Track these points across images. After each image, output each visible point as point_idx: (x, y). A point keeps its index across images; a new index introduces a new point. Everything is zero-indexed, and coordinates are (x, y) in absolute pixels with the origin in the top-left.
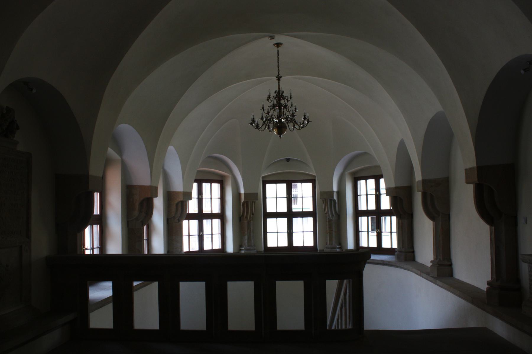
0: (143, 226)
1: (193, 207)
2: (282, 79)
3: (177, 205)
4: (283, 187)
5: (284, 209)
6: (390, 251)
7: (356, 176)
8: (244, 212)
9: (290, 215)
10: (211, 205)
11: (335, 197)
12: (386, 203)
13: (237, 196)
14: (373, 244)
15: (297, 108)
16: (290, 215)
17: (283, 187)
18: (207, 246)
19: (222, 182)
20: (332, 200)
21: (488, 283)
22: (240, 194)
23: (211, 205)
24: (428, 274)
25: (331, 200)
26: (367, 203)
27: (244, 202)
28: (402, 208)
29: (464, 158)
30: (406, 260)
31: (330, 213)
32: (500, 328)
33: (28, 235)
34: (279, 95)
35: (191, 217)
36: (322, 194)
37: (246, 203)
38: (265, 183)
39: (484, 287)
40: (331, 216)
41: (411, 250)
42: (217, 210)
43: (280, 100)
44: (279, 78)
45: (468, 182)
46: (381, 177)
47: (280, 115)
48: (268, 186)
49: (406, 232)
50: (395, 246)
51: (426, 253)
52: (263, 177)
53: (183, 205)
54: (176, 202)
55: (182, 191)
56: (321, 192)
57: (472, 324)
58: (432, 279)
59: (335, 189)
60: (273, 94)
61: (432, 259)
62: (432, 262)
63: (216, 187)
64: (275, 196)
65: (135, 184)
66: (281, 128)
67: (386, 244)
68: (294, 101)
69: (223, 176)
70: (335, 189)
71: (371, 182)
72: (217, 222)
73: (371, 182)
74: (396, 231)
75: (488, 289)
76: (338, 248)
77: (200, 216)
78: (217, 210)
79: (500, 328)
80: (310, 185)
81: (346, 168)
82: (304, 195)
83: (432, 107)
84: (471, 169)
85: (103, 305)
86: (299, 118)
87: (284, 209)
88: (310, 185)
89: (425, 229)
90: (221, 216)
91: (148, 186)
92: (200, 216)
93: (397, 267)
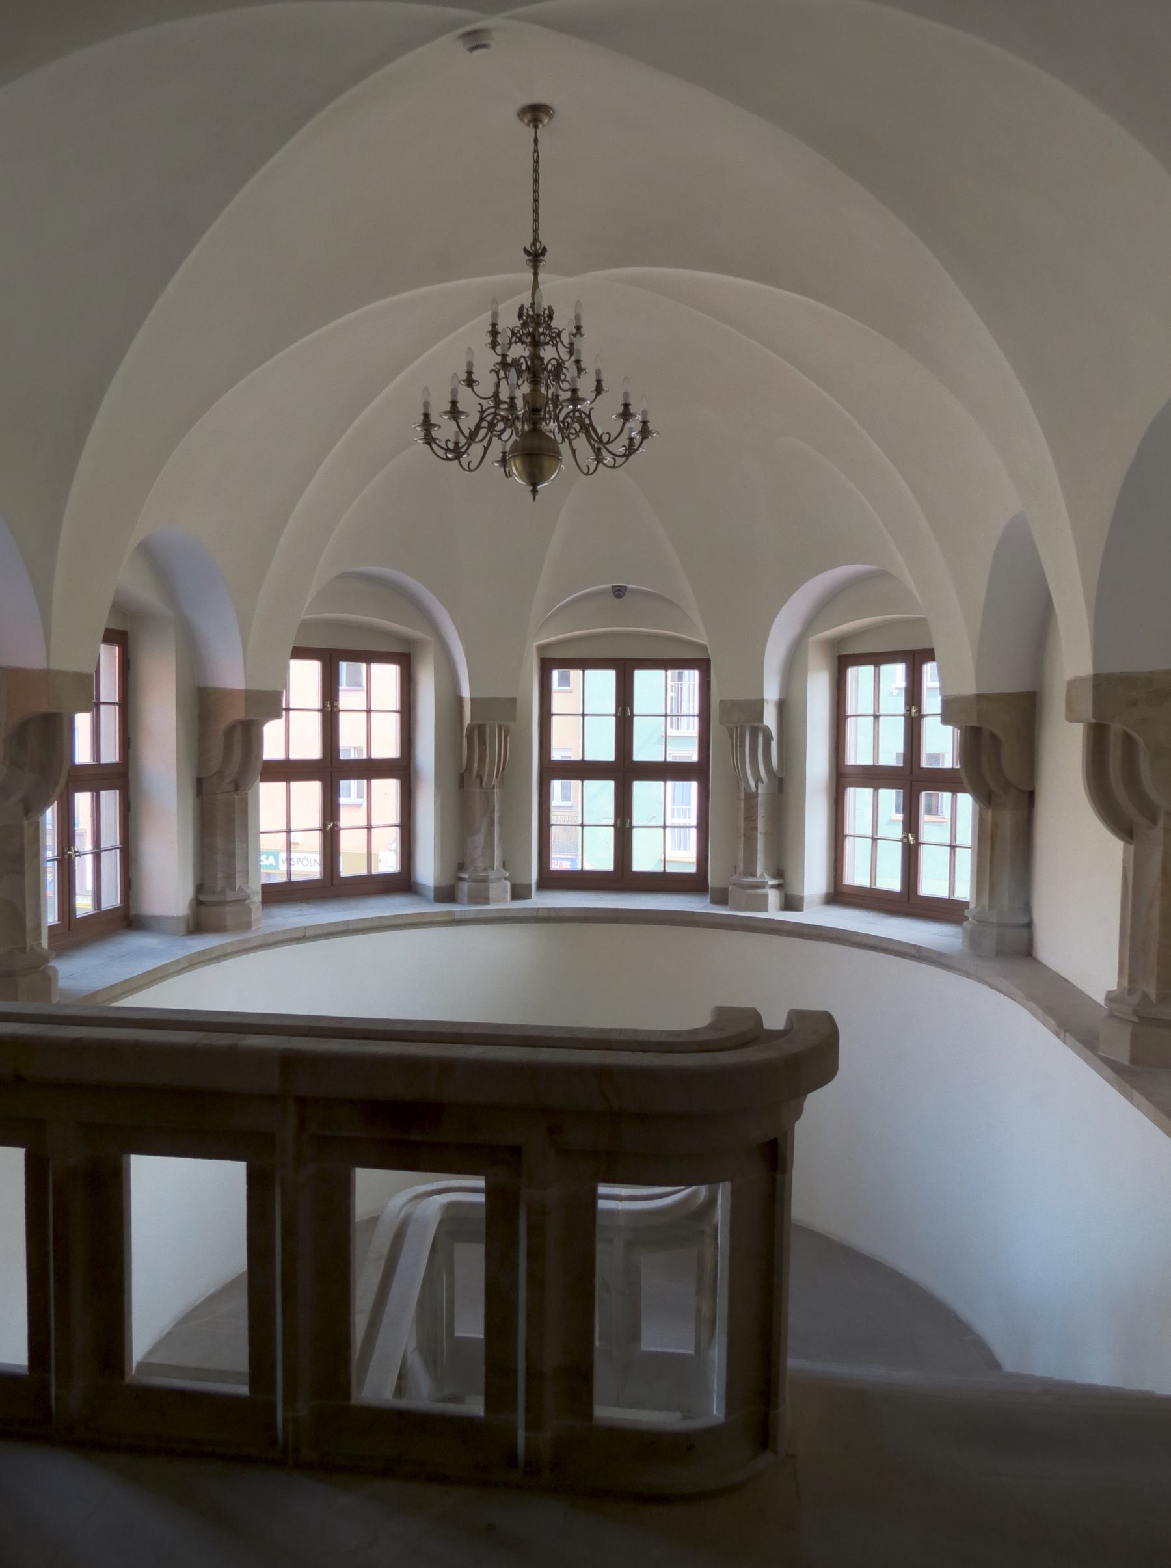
0: (32, 809)
3: (230, 732)
4: (603, 681)
6: (943, 911)
7: (548, 656)
10: (371, 731)
11: (770, 719)
12: (941, 745)
13: (450, 704)
15: (603, 377)
17: (603, 681)
19: (915, 660)
20: (757, 729)
22: (460, 700)
23: (371, 731)
25: (754, 732)
26: (876, 742)
27: (471, 729)
31: (748, 778)
34: (535, 325)
37: (478, 732)
38: (547, 665)
40: (752, 783)
41: (1025, 920)
42: (387, 747)
43: (536, 344)
47: (535, 413)
49: (1009, 846)
50: (964, 891)
52: (541, 648)
54: (224, 725)
59: (771, 693)
60: (509, 321)
61: (1113, 986)
63: (386, 676)
66: (535, 458)
67: (932, 885)
70: (771, 693)
71: (895, 675)
72: (387, 790)
73: (895, 675)
74: (969, 843)
76: (773, 887)
78: (387, 747)
80: (692, 677)
81: (813, 621)
85: (164, 978)
86: (605, 419)
88: (692, 677)
90: (401, 769)
91: (40, 671)
92: (330, 770)
93: (967, 975)
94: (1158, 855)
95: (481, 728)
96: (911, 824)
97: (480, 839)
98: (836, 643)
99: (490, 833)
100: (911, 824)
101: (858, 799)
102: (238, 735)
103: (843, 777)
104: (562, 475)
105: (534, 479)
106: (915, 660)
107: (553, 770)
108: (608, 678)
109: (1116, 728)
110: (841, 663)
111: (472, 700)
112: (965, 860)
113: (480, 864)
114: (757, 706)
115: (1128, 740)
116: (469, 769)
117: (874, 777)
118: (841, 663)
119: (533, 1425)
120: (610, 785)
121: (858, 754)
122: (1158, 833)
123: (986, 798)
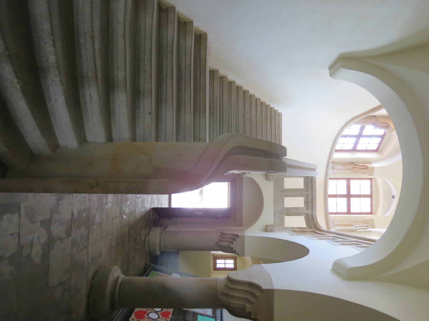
37: (367, 168)
48: (369, 181)
56: (372, 220)
64: (360, 186)
99: (342, 170)
114: (373, 227)
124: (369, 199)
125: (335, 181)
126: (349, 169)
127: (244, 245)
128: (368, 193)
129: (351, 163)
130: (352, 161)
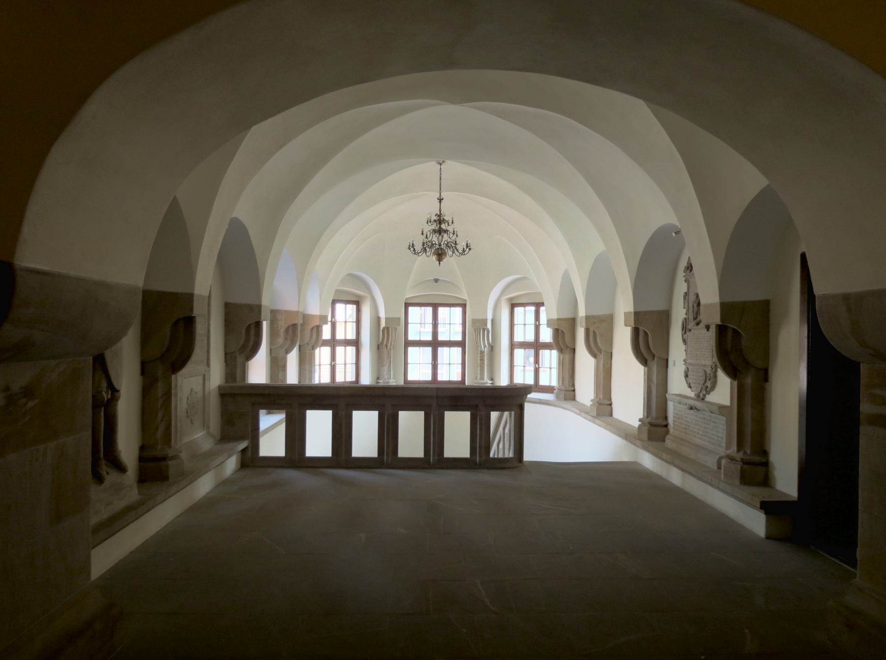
1: (326, 334)
2: (443, 202)
5: (429, 338)
6: (548, 389)
8: (383, 339)
9: (435, 344)
11: (489, 326)
12: (547, 335)
14: (530, 381)
16: (435, 344)
18: (340, 379)
19: (357, 303)
21: (640, 420)
23: (345, 331)
24: (587, 413)
25: (484, 330)
26: (525, 334)
27: (384, 329)
28: (563, 341)
29: (624, 305)
30: (565, 399)
32: (648, 461)
33: (208, 365)
34: (440, 220)
35: (325, 343)
36: (474, 321)
37: (387, 329)
39: (636, 424)
42: (351, 335)
43: (440, 223)
44: (440, 200)
45: (626, 325)
46: (542, 304)
47: (440, 241)
48: (411, 309)
49: (568, 370)
51: (586, 390)
53: (318, 329)
55: (318, 313)
56: (473, 320)
57: (625, 458)
58: (590, 418)
59: (489, 317)
61: (641, 416)
62: (592, 401)
64: (419, 323)
65: (280, 308)
66: (440, 255)
67: (544, 381)
68: (457, 227)
69: (359, 296)
70: (489, 317)
72: (351, 350)
75: (640, 426)
77: (333, 343)
79: (648, 461)
80: (459, 310)
81: (503, 293)
82: (451, 323)
83: (599, 247)
84: (629, 313)
87: (429, 338)
88: (459, 310)
89: (586, 364)
90: (356, 343)
93: (555, 406)
94: (602, 362)
95: (388, 328)
96: (537, 361)
97: (386, 368)
98: (511, 299)
99: (390, 366)
100: (537, 361)
101: (519, 353)
102: (290, 329)
103: (513, 346)
104: (446, 260)
105: (440, 260)
106: (538, 305)
107: (409, 344)
108: (429, 310)
109: (591, 329)
110: (513, 306)
111: (386, 319)
112: (555, 372)
113: (386, 377)
114: (484, 322)
115: (646, 334)
116: (382, 343)
117: (524, 345)
118: (513, 306)
119: (480, 456)
120: (430, 349)
121: (519, 338)
122: (602, 356)
123: (561, 351)
124: (441, 310)
125: (410, 367)
126: (389, 354)
127: (651, 313)
128: (429, 310)
129: (378, 348)
130: (375, 348)
